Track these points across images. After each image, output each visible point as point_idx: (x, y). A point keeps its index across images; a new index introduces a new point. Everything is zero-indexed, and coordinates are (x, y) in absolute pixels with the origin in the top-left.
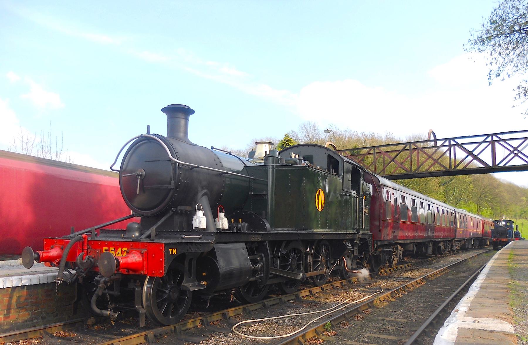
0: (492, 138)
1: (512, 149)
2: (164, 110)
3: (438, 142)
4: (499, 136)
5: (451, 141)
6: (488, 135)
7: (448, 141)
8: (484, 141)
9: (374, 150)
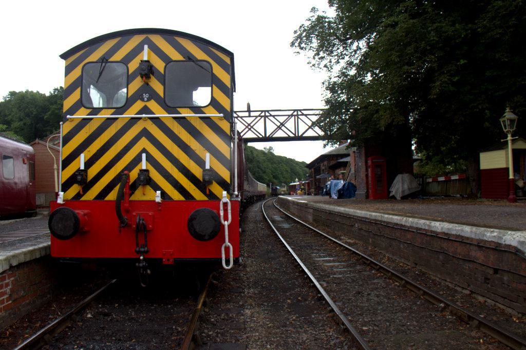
0: (297, 113)
1: (247, 125)
2: (301, 39)
3: (251, 113)
4: (270, 112)
5: (299, 112)
6: (295, 111)
7: (264, 113)
8: (259, 116)
9: (297, 113)
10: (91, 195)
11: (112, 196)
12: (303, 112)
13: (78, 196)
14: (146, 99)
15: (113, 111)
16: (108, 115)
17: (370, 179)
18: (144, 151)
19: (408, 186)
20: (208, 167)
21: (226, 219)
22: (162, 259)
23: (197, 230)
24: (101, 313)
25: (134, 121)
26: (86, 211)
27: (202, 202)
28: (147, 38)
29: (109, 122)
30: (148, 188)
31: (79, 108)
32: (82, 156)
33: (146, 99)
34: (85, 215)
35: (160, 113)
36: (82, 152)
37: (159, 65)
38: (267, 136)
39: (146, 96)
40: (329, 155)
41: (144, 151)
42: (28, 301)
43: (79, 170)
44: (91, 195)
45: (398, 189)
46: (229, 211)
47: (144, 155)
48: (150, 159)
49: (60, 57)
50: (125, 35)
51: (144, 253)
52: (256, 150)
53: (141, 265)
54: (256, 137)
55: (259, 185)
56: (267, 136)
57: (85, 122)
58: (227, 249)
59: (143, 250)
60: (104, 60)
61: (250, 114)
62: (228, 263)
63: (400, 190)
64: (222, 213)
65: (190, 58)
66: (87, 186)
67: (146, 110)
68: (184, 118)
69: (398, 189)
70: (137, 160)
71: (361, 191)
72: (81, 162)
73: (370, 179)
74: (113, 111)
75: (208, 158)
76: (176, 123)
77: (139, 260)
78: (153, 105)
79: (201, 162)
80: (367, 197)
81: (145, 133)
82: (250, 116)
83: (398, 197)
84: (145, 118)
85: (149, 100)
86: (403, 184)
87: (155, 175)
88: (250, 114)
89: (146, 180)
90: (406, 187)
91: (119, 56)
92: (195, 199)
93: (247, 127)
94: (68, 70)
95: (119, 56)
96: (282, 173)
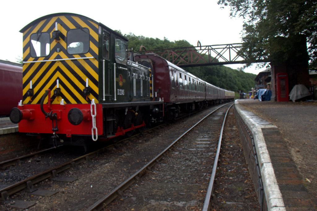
6: (227, 45)
8: (226, 48)
10: (35, 101)
11: (46, 101)
12: (233, 45)
13: (30, 102)
14: (58, 51)
15: (44, 58)
16: (42, 60)
17: (277, 88)
18: (58, 78)
19: (301, 93)
20: (87, 86)
21: (94, 114)
22: (66, 135)
23: (72, 119)
24: (35, 161)
25: (53, 63)
26: (31, 110)
27: (74, 105)
28: (58, 18)
29: (42, 64)
30: (60, 97)
31: (29, 58)
32: (31, 82)
33: (58, 51)
34: (31, 111)
35: (65, 58)
36: (31, 80)
37: (64, 32)
38: (231, 60)
39: (58, 49)
40: (170, 79)
41: (58, 78)
42: (7, 153)
43: (30, 89)
44: (35, 101)
45: (294, 95)
46: (95, 110)
47: (58, 81)
48: (61, 83)
49: (19, 32)
50: (48, 18)
51: (55, 131)
52: (232, 70)
53: (54, 137)
54: (225, 61)
55: (226, 92)
56: (231, 60)
57: (32, 65)
58: (94, 130)
59: (55, 129)
60: (39, 31)
61: (201, 48)
62: (95, 138)
63: (295, 96)
64: (92, 111)
65: (78, 26)
66: (34, 97)
67: (58, 57)
68: (76, 60)
69: (294, 95)
70: (55, 83)
71: (273, 97)
72: (30, 85)
73: (277, 88)
74: (44, 58)
75: (87, 80)
76: (72, 63)
77: (53, 135)
78: (62, 54)
79: (84, 83)
80: (276, 100)
81: (58, 69)
82: (201, 50)
83: (294, 101)
84: (58, 61)
85: (60, 51)
86: (297, 91)
87: (63, 91)
88: (201, 48)
89: (59, 94)
90: (299, 93)
91: (45, 30)
92: (71, 103)
93: (218, 55)
94: (24, 38)
95: (45, 30)
96: (249, 84)
